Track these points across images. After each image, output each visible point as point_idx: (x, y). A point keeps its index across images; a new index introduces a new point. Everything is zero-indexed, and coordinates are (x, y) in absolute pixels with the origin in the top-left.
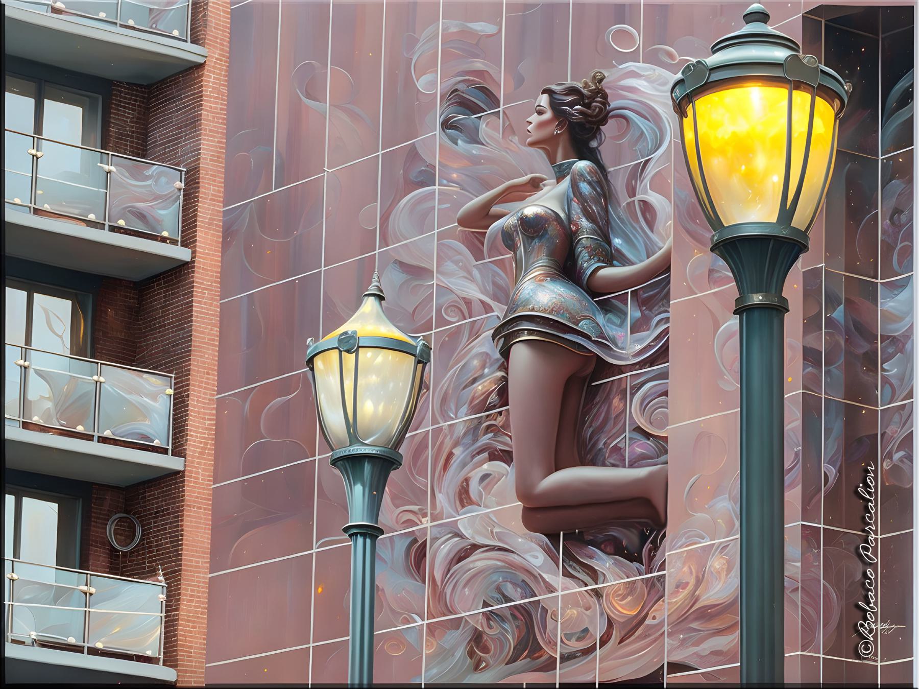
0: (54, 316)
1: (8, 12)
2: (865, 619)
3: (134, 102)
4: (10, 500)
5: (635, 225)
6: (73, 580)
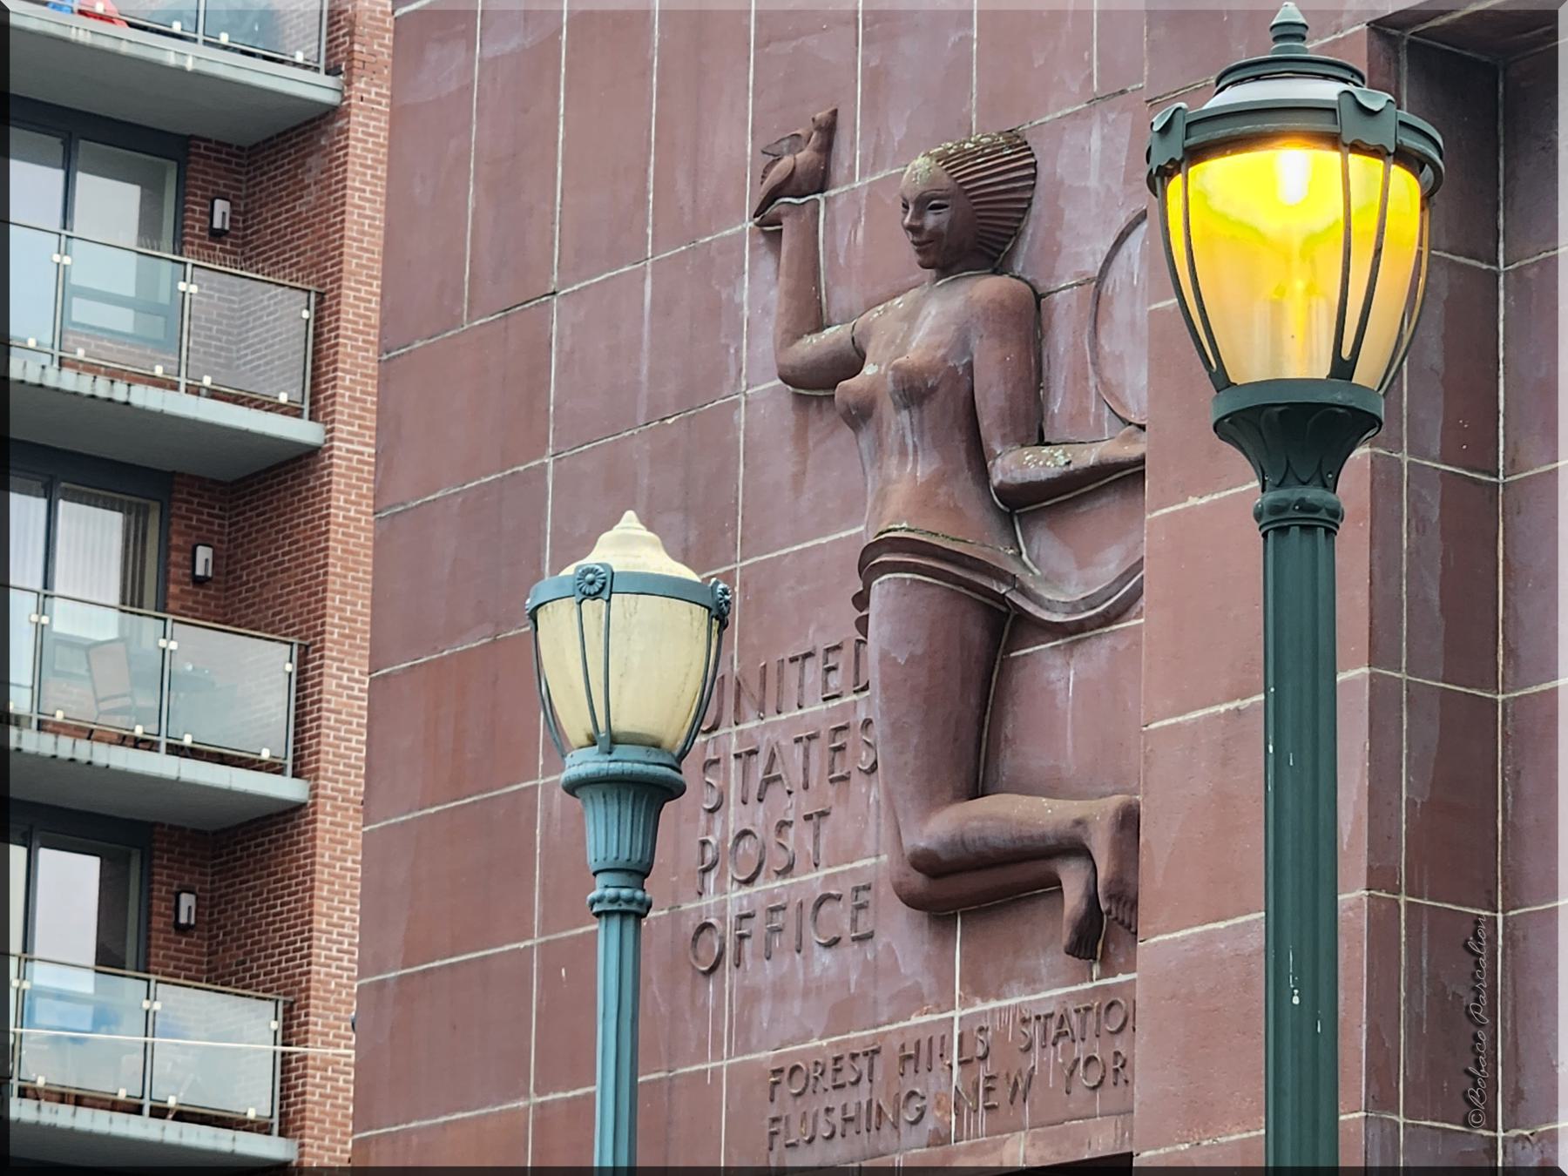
0: (92, 538)
1: (14, 20)
2: (1476, 1086)
3: (233, 172)
4: (17, 854)
5: (987, 601)
6: (129, 990)
